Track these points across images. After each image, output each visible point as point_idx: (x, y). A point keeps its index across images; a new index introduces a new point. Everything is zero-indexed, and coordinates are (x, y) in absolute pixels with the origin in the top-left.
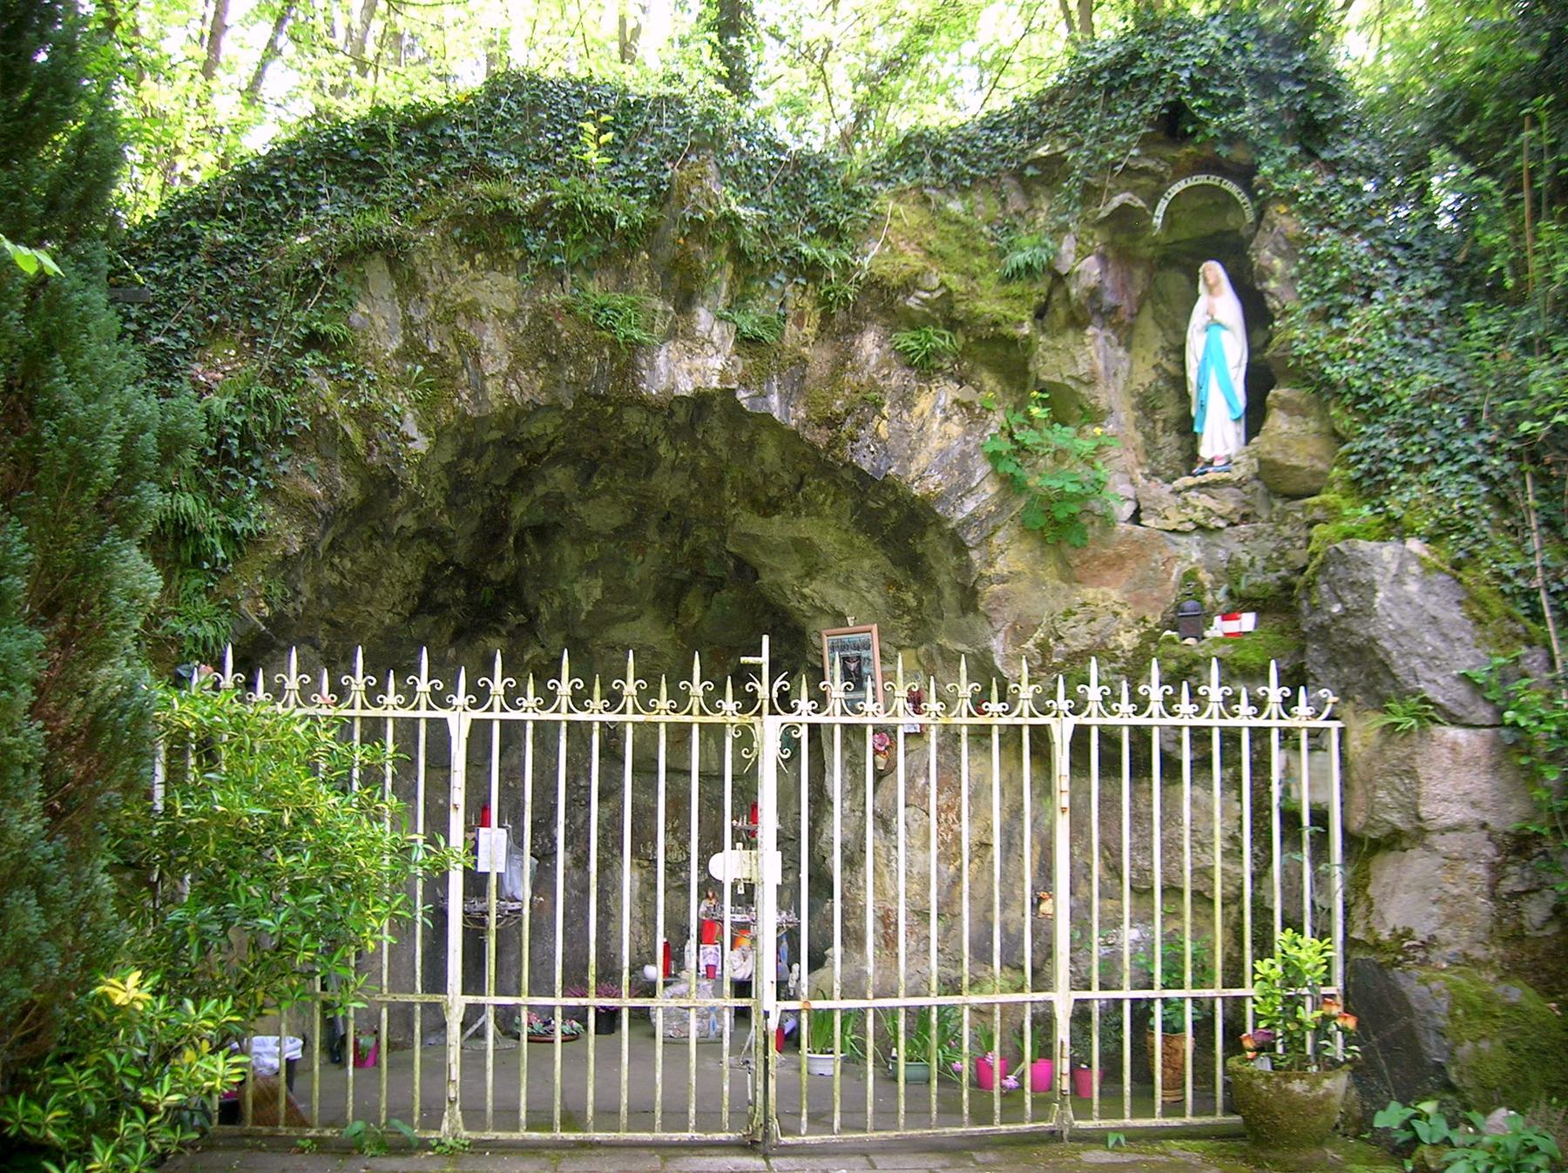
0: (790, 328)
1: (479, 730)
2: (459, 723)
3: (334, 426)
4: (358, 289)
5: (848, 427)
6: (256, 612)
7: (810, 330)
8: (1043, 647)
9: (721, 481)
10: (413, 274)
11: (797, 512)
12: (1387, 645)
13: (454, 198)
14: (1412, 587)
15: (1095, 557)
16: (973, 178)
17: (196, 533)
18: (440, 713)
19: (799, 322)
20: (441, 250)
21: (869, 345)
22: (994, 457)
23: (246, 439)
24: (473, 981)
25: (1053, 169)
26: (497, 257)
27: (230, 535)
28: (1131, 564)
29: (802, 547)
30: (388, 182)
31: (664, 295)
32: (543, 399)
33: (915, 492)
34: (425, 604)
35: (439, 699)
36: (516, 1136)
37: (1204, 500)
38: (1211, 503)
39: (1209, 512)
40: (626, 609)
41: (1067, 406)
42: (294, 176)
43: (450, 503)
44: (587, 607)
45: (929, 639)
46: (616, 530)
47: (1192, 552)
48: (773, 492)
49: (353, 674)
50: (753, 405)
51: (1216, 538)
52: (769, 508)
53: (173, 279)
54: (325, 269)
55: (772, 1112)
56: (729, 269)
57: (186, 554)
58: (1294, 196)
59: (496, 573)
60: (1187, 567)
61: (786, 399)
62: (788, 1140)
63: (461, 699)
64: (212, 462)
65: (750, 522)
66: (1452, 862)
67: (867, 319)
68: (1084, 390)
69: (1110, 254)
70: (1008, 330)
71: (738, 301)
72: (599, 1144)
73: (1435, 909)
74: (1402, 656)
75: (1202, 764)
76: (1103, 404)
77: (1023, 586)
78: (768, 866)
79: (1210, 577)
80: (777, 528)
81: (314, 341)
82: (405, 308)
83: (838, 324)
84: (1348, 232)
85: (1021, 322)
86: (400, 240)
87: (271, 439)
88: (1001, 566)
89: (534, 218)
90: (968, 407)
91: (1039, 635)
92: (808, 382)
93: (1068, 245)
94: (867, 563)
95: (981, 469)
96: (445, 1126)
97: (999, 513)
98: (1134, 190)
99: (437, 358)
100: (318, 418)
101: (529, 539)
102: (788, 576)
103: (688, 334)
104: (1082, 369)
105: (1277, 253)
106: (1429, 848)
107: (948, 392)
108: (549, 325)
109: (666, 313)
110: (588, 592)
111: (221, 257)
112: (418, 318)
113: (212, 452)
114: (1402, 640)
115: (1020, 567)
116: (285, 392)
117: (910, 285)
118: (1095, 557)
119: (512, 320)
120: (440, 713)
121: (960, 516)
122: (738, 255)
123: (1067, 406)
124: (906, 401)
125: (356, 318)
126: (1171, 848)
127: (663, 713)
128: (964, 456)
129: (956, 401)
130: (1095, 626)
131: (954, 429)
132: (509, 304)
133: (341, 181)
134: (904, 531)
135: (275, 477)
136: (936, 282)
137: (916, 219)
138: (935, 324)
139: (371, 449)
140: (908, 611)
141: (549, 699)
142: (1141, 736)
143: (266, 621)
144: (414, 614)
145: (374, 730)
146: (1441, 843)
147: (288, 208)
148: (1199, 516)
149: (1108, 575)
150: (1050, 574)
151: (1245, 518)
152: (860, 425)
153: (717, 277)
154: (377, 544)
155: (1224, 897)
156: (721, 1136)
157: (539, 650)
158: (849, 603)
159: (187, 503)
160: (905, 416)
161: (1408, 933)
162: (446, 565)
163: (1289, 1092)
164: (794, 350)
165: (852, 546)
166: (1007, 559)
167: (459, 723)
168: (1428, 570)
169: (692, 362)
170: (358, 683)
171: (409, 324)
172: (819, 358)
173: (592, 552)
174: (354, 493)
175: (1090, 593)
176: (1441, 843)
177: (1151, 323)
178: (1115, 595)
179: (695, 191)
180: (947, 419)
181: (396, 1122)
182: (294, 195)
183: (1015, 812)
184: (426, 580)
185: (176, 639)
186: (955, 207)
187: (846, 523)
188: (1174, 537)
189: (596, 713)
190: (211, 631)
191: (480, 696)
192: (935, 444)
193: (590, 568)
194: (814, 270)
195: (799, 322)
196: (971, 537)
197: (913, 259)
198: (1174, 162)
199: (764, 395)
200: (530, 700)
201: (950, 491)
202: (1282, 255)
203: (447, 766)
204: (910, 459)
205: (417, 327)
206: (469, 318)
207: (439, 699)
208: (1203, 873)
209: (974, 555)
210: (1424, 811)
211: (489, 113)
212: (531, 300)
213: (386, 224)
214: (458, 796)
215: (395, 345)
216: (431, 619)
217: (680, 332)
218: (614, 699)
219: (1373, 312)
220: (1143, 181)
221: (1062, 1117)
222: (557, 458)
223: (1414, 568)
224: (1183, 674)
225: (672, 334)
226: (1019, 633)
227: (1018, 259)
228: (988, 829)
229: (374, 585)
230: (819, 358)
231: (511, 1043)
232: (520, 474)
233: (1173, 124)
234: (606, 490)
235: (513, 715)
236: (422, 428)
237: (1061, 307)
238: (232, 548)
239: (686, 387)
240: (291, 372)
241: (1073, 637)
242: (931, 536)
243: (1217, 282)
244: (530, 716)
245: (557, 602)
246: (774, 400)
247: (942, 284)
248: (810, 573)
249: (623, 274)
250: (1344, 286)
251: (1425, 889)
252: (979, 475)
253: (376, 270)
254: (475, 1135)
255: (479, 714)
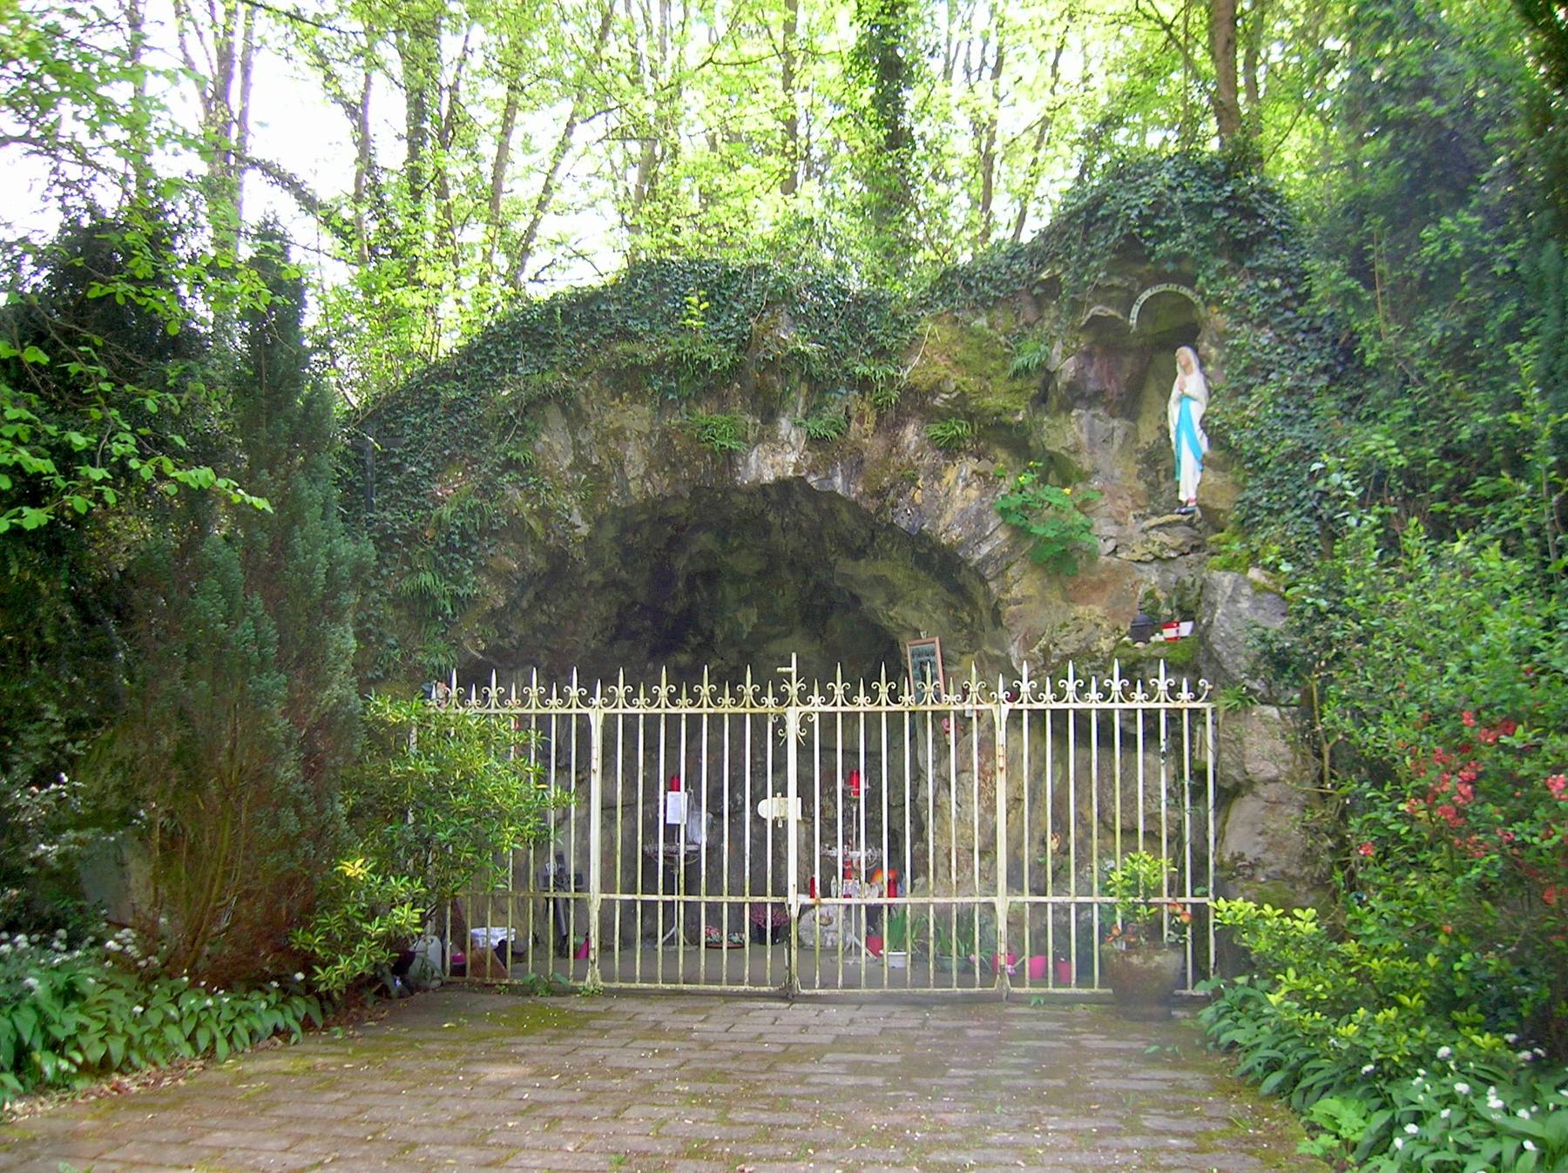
0: (854, 425)
1: (609, 721)
2: (596, 719)
3: (522, 521)
4: (541, 425)
5: (891, 497)
6: (475, 650)
7: (869, 426)
8: (1045, 652)
9: (820, 536)
10: (579, 410)
11: (876, 557)
12: (1218, 648)
13: (604, 357)
14: (1244, 605)
15: (1084, 582)
16: (996, 299)
17: (434, 598)
18: (585, 710)
19: (861, 420)
20: (598, 393)
21: (910, 435)
22: (1004, 512)
23: (464, 535)
24: (607, 886)
25: (1053, 284)
26: (638, 395)
27: (455, 597)
28: (1110, 588)
29: (880, 581)
30: (559, 350)
31: (754, 412)
32: (669, 492)
33: (944, 542)
34: (620, 631)
35: (584, 701)
36: (633, 986)
37: (1162, 537)
38: (1166, 539)
39: (1163, 546)
40: (778, 629)
41: (1058, 469)
42: (500, 347)
43: (624, 564)
44: (747, 629)
45: (980, 647)
46: (758, 573)
47: (1152, 577)
48: (858, 542)
49: (1157, 677)
50: (821, 485)
51: (1170, 565)
52: (857, 554)
53: (422, 426)
54: (517, 414)
55: (794, 971)
56: (804, 388)
57: (429, 611)
58: (1220, 300)
59: (673, 608)
60: (1148, 588)
61: (847, 480)
62: (806, 992)
63: (597, 701)
64: (443, 552)
65: (845, 566)
66: (1273, 804)
67: (909, 415)
68: (1073, 458)
69: (1098, 350)
70: (1007, 418)
71: (813, 410)
72: (689, 993)
73: (1260, 839)
74: (1230, 655)
75: (1151, 735)
76: (1087, 467)
77: (1033, 606)
78: (792, 807)
79: (1164, 595)
80: (863, 569)
81: (510, 464)
82: (573, 433)
83: (889, 423)
84: (1260, 326)
85: (1017, 411)
86: (567, 390)
87: (481, 533)
88: (1016, 592)
89: (659, 365)
90: (984, 475)
91: (1043, 642)
92: (866, 464)
93: (1058, 348)
94: (930, 592)
95: (993, 522)
96: (589, 978)
97: (1011, 553)
98: (1108, 303)
99: (597, 468)
100: (513, 518)
101: (698, 582)
102: (878, 602)
103: (773, 438)
104: (1070, 441)
105: (1212, 343)
106: (1256, 794)
107: (969, 465)
108: (670, 441)
109: (755, 425)
110: (748, 618)
111: (454, 408)
112: (584, 441)
113: (442, 545)
114: (1231, 644)
115: (1031, 591)
116: (491, 501)
117: (935, 389)
118: (1084, 582)
119: (648, 438)
120: (585, 710)
121: (977, 557)
122: (808, 377)
123: (1058, 469)
124: (936, 474)
125: (539, 446)
126: (1129, 801)
127: (727, 707)
128: (980, 513)
129: (974, 472)
130: (1082, 635)
131: (973, 493)
132: (645, 427)
133: (532, 348)
134: (943, 566)
135: (486, 558)
136: (953, 386)
137: (947, 336)
138: (958, 416)
139: (548, 536)
140: (965, 626)
141: (653, 699)
142: (1106, 717)
143: (483, 653)
144: (614, 639)
145: (544, 721)
146: (1264, 792)
147: (497, 370)
148: (1156, 549)
149: (1094, 596)
150: (1055, 597)
151: (1194, 549)
152: (899, 495)
153: (793, 395)
154: (574, 594)
155: (1168, 837)
156: (765, 989)
157: (719, 661)
158: (922, 626)
159: (426, 578)
160: (936, 485)
161: (1241, 856)
162: (634, 603)
163: (1129, 965)
164: (856, 441)
165: (917, 579)
166: (1022, 585)
167: (596, 719)
168: (1258, 591)
169: (774, 460)
170: (749, 690)
171: (577, 445)
172: (874, 446)
173: (746, 589)
174: (542, 564)
175: (1081, 610)
176: (1264, 792)
177: (1156, 393)
178: (1098, 610)
179: (767, 338)
180: (968, 485)
181: (558, 975)
182: (502, 360)
183: (1038, 775)
184: (619, 615)
185: (421, 667)
186: (981, 322)
187: (910, 564)
188: (1139, 566)
189: (684, 708)
190: (444, 661)
191: (610, 699)
192: (959, 505)
193: (746, 601)
194: (865, 384)
195: (861, 422)
196: (989, 572)
197: (941, 368)
198: (1140, 277)
199: (829, 478)
200: (642, 700)
201: (968, 540)
202: (1216, 345)
203: (589, 748)
204: (939, 517)
205: (583, 448)
206: (617, 439)
207: (584, 701)
208: (1152, 817)
209: (992, 585)
210: (1249, 768)
211: (630, 290)
212: (659, 423)
213: (555, 380)
214: (596, 764)
215: (568, 462)
216: (628, 643)
217: (767, 436)
218: (695, 698)
219: (1268, 391)
220: (1114, 294)
221: (1002, 985)
222: (697, 528)
223: (1247, 590)
224: (1134, 672)
225: (760, 439)
226: (1028, 643)
227: (1019, 361)
228: (1020, 788)
229: (576, 622)
230: (874, 446)
231: (694, 948)
232: (672, 540)
233: (1131, 250)
234: (741, 546)
235: (630, 710)
236: (584, 518)
237: (1046, 393)
238: (458, 606)
239: (769, 477)
240: (495, 487)
241: (1066, 643)
242: (964, 572)
243: (1188, 363)
244: (642, 711)
245: (727, 625)
246: (839, 480)
247: (957, 388)
248: (892, 600)
249: (722, 399)
250: (1248, 371)
251: (1253, 824)
252: (991, 526)
253: (553, 413)
254: (606, 985)
255: (609, 710)
